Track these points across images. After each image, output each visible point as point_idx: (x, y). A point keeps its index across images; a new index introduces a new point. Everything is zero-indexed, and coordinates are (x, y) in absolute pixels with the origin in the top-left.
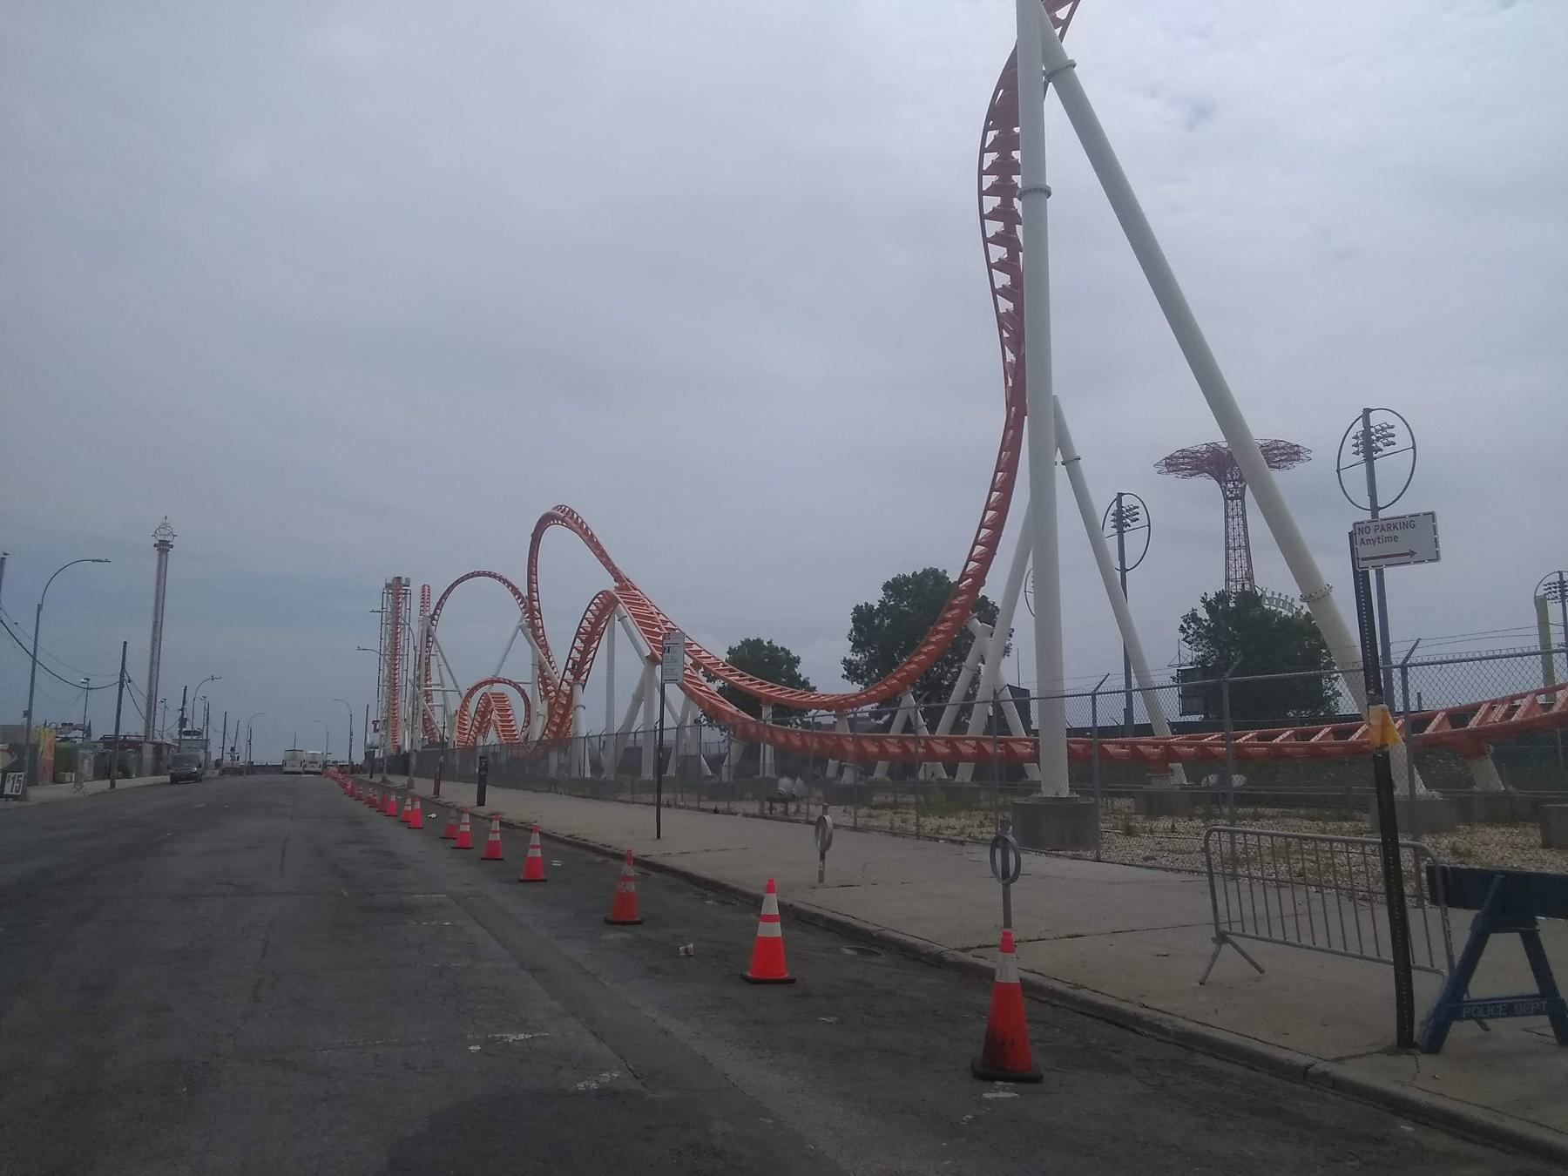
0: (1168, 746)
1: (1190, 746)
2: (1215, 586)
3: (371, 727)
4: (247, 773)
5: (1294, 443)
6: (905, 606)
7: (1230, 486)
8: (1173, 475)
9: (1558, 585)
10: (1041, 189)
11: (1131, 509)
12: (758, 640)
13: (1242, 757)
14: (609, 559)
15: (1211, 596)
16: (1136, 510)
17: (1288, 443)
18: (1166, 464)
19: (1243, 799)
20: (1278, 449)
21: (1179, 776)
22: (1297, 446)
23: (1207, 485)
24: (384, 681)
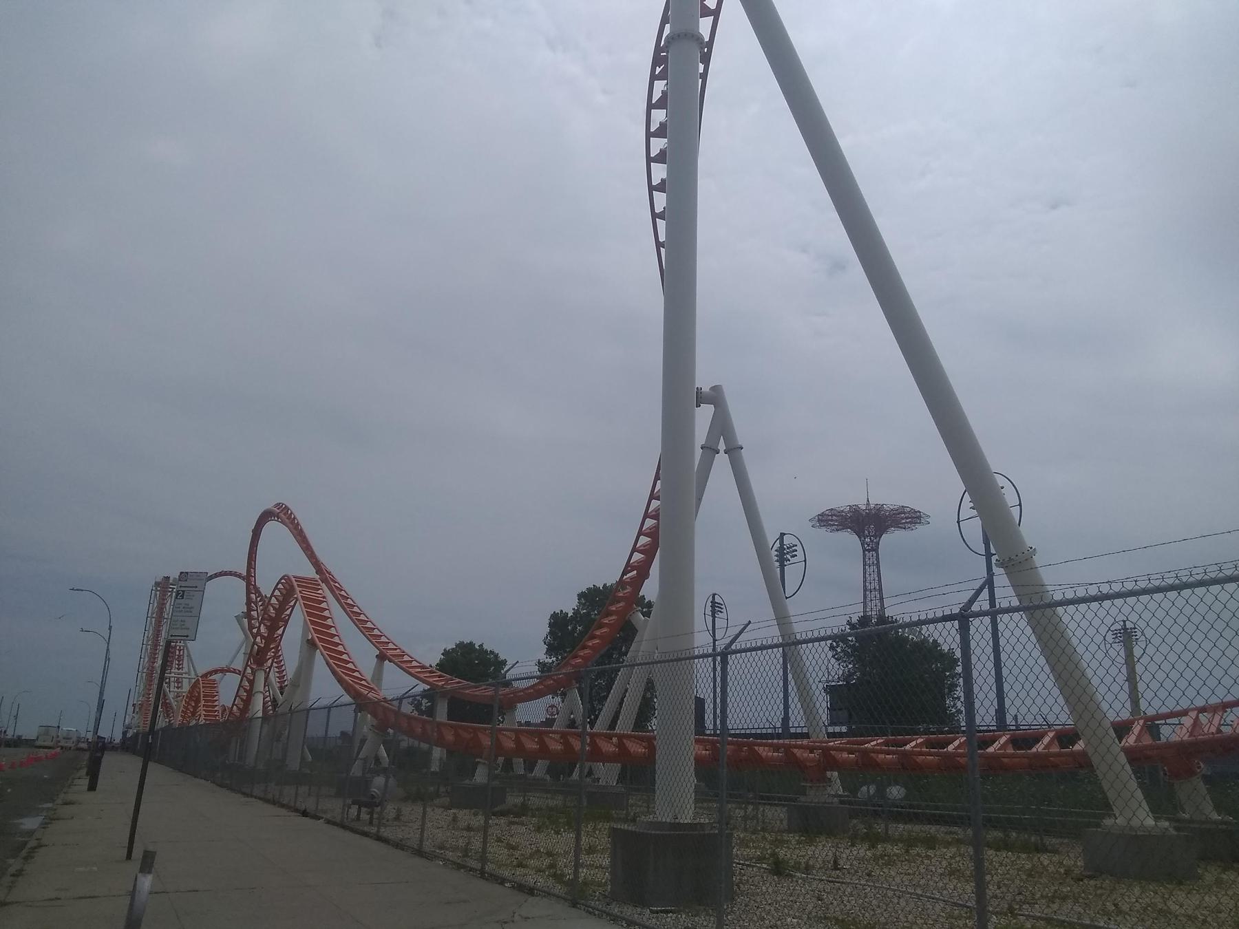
0: (826, 751)
1: (893, 753)
2: (856, 613)
3: (131, 709)
4: (15, 747)
5: (917, 509)
6: (596, 614)
7: (868, 540)
8: (824, 529)
9: (1122, 631)
10: (693, 36)
11: (791, 547)
12: (471, 643)
13: (908, 768)
14: (313, 552)
15: (855, 620)
16: (795, 548)
17: (912, 509)
18: (819, 520)
19: (899, 815)
20: (904, 513)
21: (836, 784)
22: (920, 512)
23: (850, 540)
24: (143, 669)
